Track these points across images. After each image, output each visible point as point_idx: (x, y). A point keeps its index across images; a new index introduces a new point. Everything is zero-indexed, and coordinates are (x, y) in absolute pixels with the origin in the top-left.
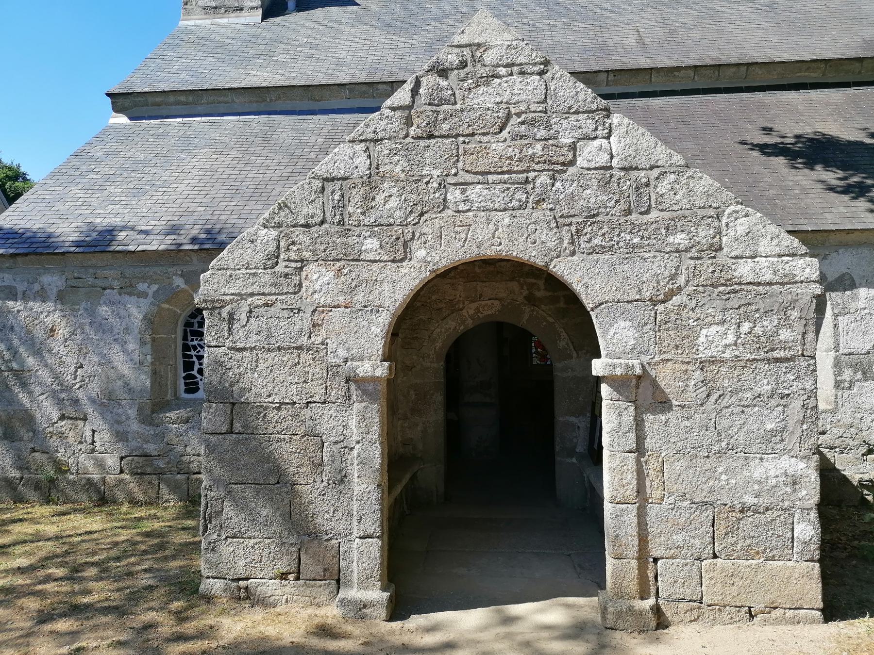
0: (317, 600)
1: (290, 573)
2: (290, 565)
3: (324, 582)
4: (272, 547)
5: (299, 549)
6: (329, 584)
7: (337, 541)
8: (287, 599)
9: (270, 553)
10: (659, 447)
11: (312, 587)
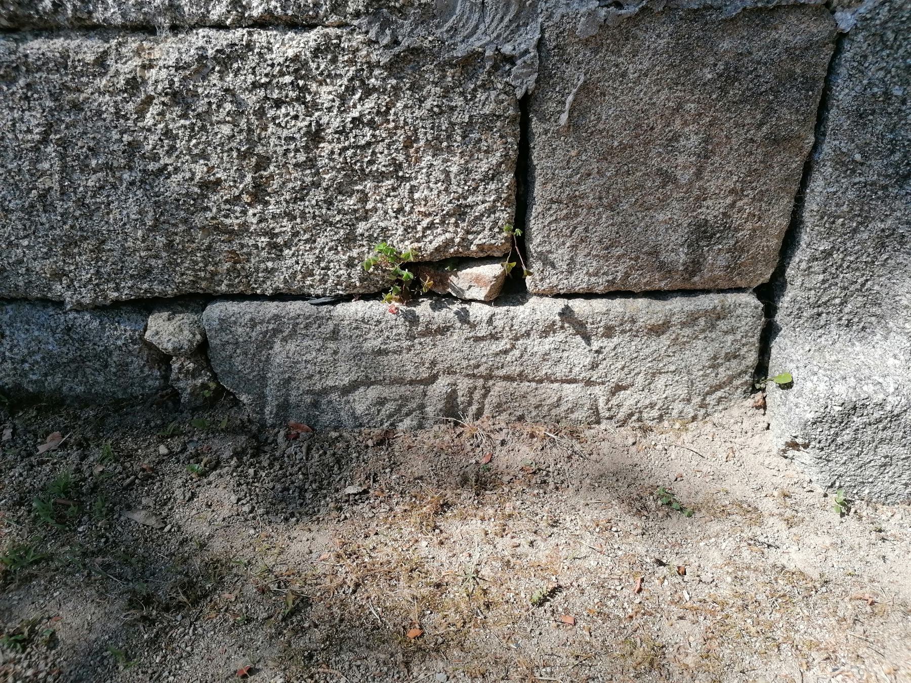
0: (628, 400)
1: (463, 261)
2: (460, 212)
3: (677, 304)
4: (325, 94)
5: (525, 104)
6: (717, 316)
7: (819, 29)
8: (451, 397)
9: (315, 136)
10: (819, 315)
11: (609, 332)
